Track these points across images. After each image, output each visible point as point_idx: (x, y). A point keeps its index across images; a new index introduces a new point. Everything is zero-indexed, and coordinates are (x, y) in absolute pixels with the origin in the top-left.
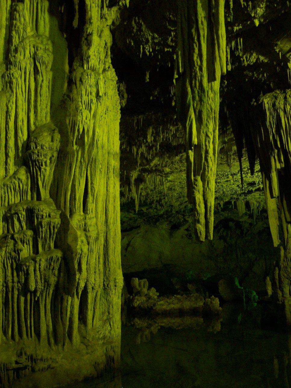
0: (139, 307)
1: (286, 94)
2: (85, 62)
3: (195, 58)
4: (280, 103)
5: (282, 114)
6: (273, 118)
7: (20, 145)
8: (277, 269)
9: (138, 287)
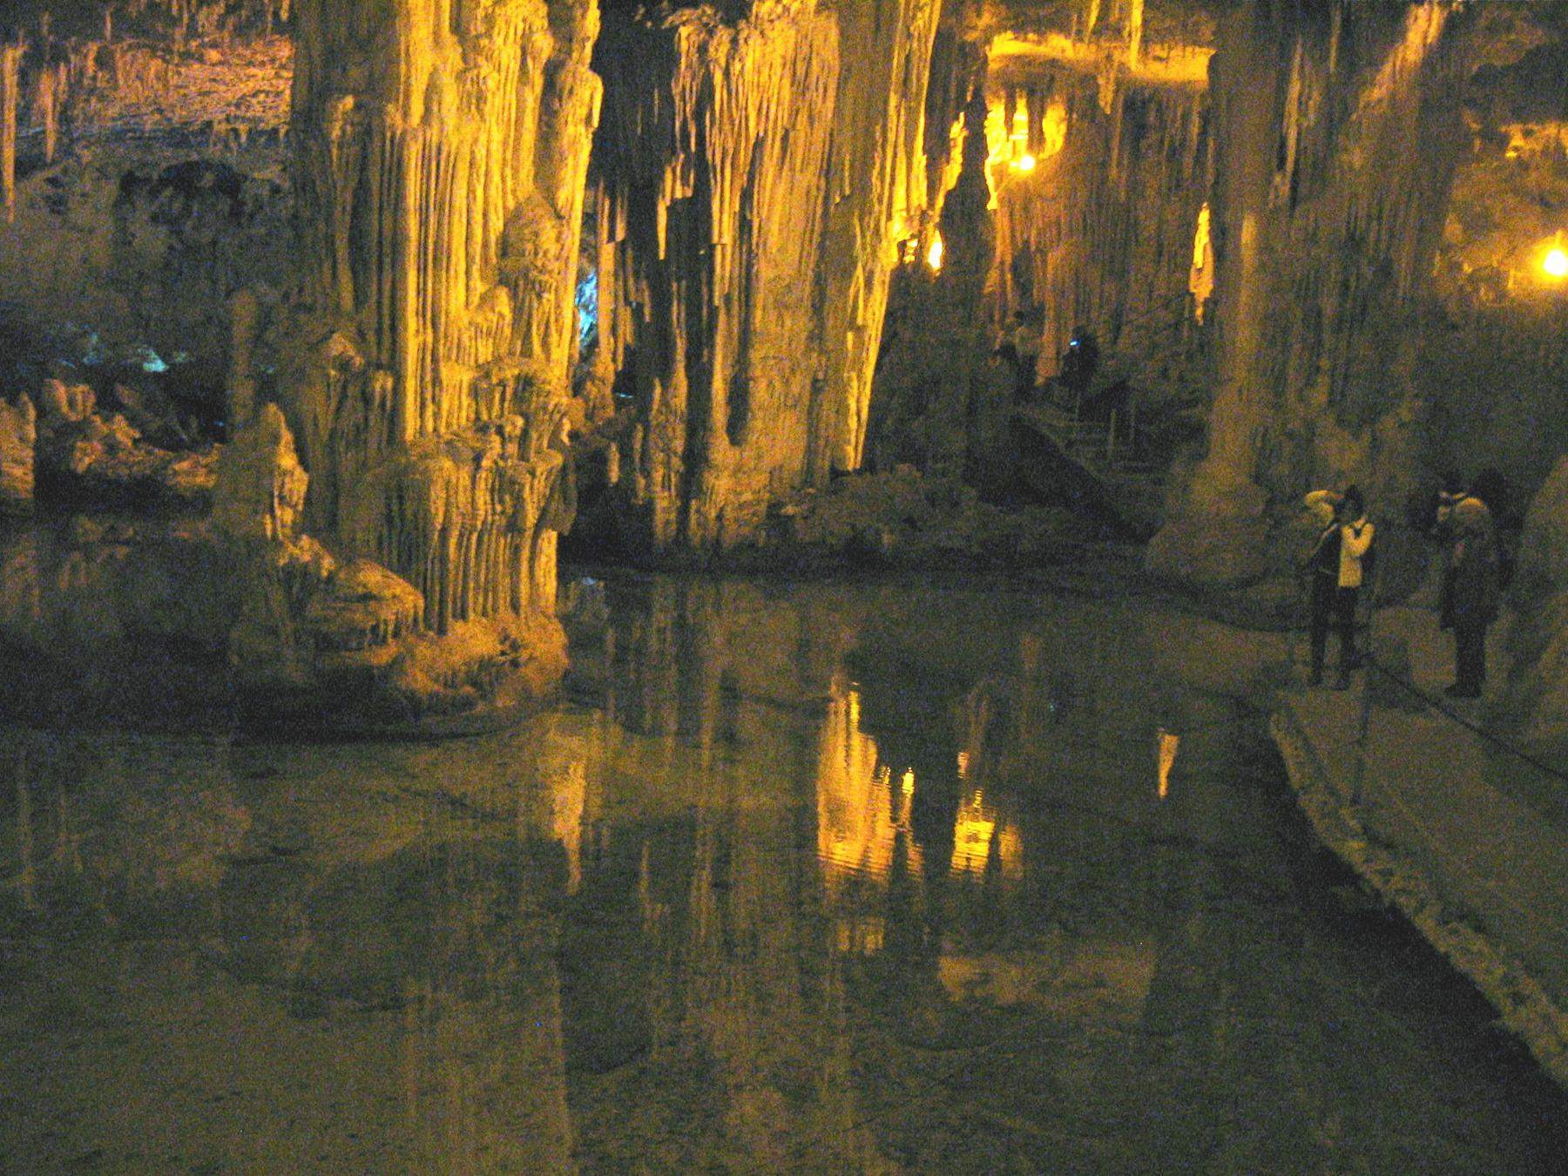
1: (738, 33)
2: (575, 46)
3: (874, 180)
4: (719, 49)
5: (718, 77)
6: (693, 79)
7: (493, 237)
8: (639, 427)
9: (65, 409)
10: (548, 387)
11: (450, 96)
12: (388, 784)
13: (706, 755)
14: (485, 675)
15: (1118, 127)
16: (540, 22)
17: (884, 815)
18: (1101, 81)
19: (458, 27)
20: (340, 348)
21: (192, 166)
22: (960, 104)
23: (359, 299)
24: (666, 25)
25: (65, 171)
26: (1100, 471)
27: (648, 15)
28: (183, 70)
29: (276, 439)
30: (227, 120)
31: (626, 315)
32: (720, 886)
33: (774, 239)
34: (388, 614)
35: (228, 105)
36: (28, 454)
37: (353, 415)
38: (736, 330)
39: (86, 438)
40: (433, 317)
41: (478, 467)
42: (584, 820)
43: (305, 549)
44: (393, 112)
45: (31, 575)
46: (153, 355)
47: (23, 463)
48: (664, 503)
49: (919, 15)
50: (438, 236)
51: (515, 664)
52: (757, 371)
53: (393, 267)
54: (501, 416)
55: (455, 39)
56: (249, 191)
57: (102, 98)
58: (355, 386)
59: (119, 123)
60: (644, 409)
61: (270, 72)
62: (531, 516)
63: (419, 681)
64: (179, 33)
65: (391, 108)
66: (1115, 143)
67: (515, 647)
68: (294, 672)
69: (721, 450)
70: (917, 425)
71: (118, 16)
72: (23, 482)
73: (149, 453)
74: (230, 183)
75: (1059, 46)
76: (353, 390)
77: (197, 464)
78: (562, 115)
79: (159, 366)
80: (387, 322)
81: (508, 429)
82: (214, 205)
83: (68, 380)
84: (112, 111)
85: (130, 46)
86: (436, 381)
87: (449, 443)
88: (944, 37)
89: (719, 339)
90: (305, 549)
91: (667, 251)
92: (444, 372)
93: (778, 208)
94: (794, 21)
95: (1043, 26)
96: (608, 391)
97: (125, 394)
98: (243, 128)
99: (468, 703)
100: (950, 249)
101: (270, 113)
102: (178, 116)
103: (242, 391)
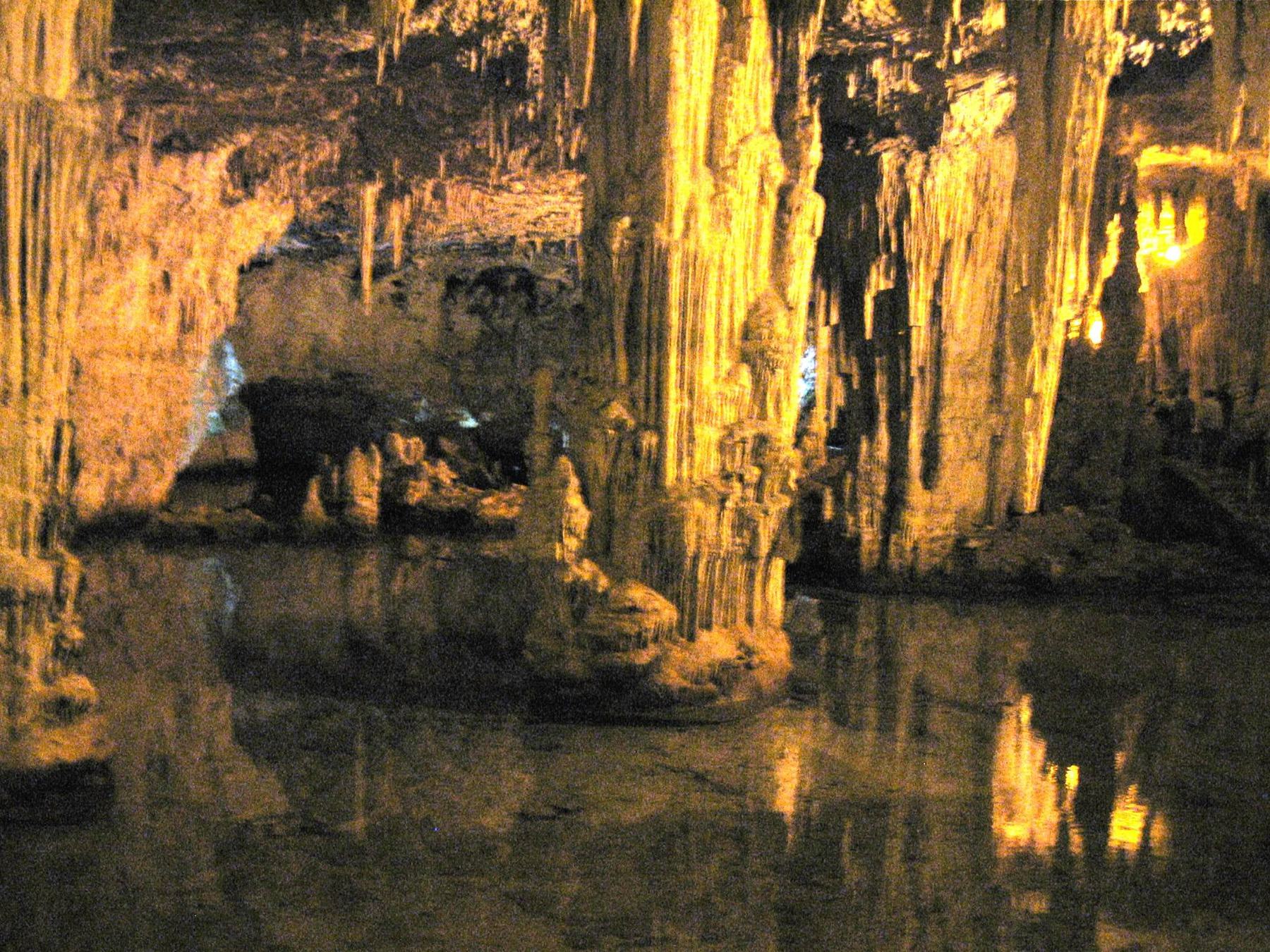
0: (420, 504)
1: (930, 156)
2: (802, 172)
4: (915, 169)
5: (914, 192)
9: (403, 456)
10: (778, 444)
11: (705, 215)
12: (644, 760)
13: (899, 747)
14: (724, 676)
15: (1251, 222)
16: (775, 154)
17: (1050, 800)
18: (1237, 183)
19: (710, 161)
20: (616, 413)
21: (499, 270)
22: (1115, 208)
23: (633, 374)
24: (872, 152)
25: (406, 275)
26: (795, 344)
27: (857, 146)
28: (495, 198)
29: (565, 484)
30: (527, 235)
31: (838, 384)
32: (909, 858)
33: (960, 325)
34: (650, 623)
35: (528, 223)
36: (375, 490)
37: (625, 464)
38: (928, 395)
39: (417, 479)
40: (690, 389)
41: (723, 508)
42: (799, 795)
43: (587, 570)
44: (660, 232)
45: (375, 583)
46: (467, 415)
47: (369, 496)
48: (869, 536)
49: (1084, 137)
50: (694, 325)
51: (749, 667)
52: (946, 430)
53: (659, 351)
54: (742, 466)
55: (707, 170)
56: (542, 287)
57: (436, 220)
58: (627, 443)
59: (446, 239)
60: (854, 456)
61: (560, 197)
62: (764, 547)
63: (672, 678)
64: (493, 172)
65: (658, 225)
66: (1249, 235)
67: (750, 652)
68: (575, 666)
69: (916, 493)
70: (1081, 475)
71: (450, 159)
72: (372, 511)
73: (464, 490)
74: (527, 282)
75: (1199, 155)
76: (626, 445)
77: (499, 499)
78: (791, 229)
79: (471, 423)
80: (653, 392)
81: (747, 477)
82: (515, 299)
83: (407, 432)
84: (442, 230)
85: (457, 182)
86: (692, 439)
87: (701, 488)
88: (1104, 152)
89: (915, 403)
90: (587, 570)
91: (874, 329)
92: (698, 430)
93: (964, 295)
94: (976, 146)
95: (1185, 140)
96: (821, 445)
97: (446, 444)
98: (538, 241)
99: (711, 697)
100: (1109, 327)
101: (559, 229)
102: (491, 231)
103: (538, 447)
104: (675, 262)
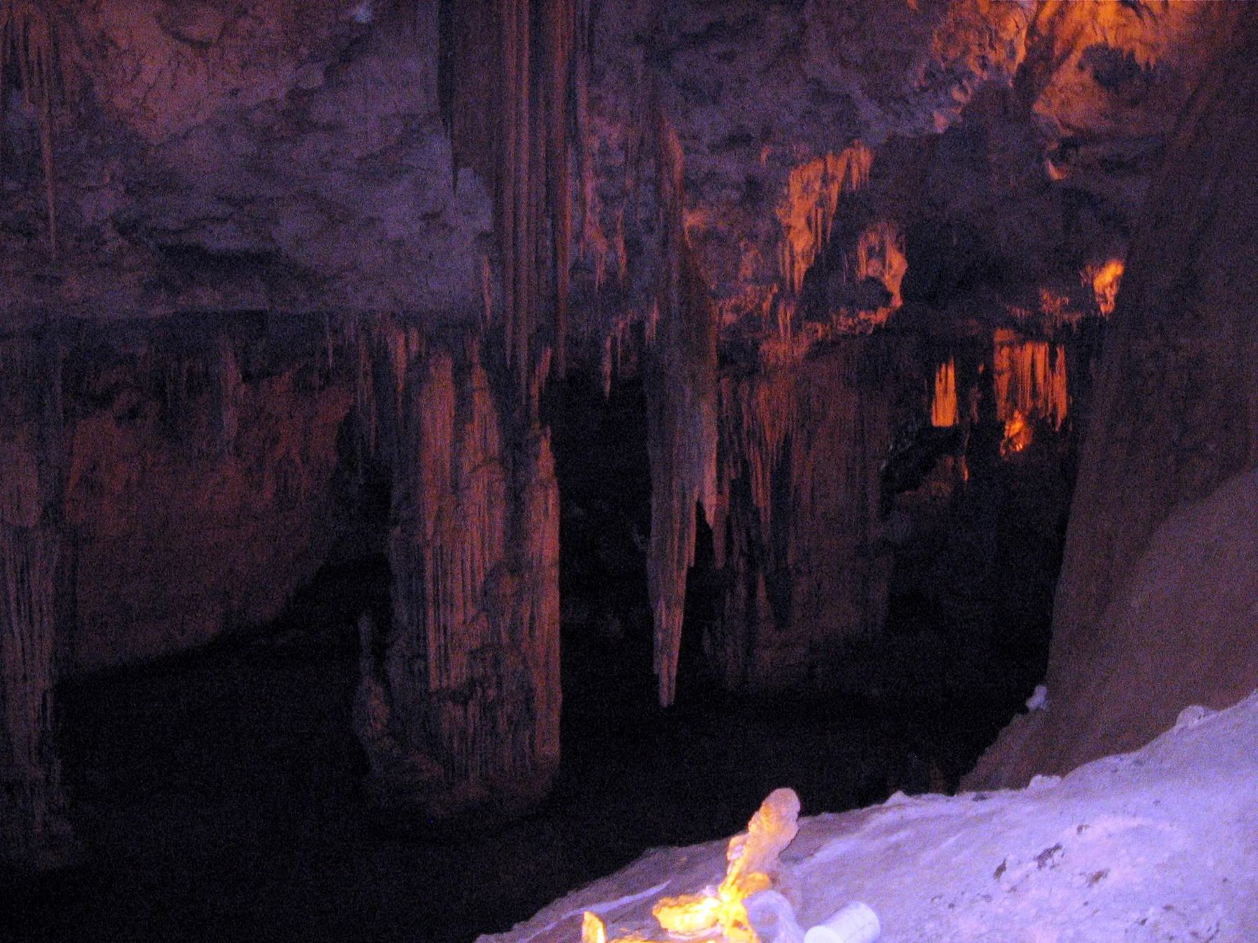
5: (744, 407)
104: (428, 554)
